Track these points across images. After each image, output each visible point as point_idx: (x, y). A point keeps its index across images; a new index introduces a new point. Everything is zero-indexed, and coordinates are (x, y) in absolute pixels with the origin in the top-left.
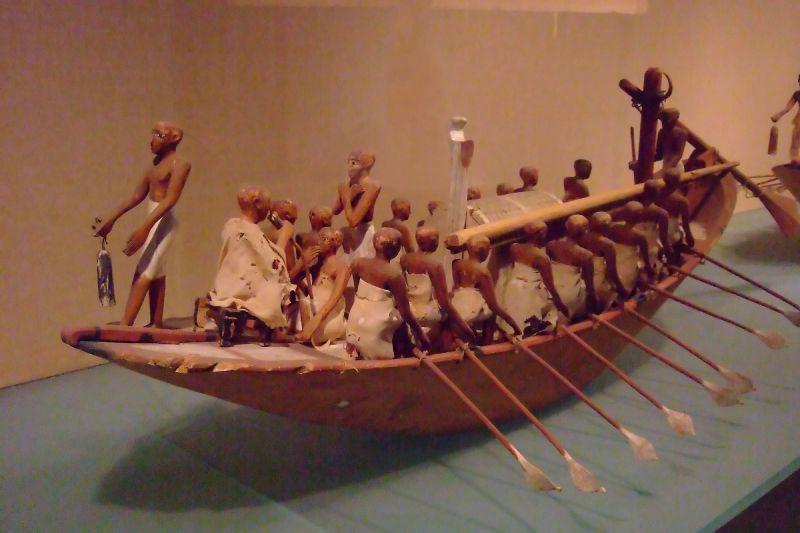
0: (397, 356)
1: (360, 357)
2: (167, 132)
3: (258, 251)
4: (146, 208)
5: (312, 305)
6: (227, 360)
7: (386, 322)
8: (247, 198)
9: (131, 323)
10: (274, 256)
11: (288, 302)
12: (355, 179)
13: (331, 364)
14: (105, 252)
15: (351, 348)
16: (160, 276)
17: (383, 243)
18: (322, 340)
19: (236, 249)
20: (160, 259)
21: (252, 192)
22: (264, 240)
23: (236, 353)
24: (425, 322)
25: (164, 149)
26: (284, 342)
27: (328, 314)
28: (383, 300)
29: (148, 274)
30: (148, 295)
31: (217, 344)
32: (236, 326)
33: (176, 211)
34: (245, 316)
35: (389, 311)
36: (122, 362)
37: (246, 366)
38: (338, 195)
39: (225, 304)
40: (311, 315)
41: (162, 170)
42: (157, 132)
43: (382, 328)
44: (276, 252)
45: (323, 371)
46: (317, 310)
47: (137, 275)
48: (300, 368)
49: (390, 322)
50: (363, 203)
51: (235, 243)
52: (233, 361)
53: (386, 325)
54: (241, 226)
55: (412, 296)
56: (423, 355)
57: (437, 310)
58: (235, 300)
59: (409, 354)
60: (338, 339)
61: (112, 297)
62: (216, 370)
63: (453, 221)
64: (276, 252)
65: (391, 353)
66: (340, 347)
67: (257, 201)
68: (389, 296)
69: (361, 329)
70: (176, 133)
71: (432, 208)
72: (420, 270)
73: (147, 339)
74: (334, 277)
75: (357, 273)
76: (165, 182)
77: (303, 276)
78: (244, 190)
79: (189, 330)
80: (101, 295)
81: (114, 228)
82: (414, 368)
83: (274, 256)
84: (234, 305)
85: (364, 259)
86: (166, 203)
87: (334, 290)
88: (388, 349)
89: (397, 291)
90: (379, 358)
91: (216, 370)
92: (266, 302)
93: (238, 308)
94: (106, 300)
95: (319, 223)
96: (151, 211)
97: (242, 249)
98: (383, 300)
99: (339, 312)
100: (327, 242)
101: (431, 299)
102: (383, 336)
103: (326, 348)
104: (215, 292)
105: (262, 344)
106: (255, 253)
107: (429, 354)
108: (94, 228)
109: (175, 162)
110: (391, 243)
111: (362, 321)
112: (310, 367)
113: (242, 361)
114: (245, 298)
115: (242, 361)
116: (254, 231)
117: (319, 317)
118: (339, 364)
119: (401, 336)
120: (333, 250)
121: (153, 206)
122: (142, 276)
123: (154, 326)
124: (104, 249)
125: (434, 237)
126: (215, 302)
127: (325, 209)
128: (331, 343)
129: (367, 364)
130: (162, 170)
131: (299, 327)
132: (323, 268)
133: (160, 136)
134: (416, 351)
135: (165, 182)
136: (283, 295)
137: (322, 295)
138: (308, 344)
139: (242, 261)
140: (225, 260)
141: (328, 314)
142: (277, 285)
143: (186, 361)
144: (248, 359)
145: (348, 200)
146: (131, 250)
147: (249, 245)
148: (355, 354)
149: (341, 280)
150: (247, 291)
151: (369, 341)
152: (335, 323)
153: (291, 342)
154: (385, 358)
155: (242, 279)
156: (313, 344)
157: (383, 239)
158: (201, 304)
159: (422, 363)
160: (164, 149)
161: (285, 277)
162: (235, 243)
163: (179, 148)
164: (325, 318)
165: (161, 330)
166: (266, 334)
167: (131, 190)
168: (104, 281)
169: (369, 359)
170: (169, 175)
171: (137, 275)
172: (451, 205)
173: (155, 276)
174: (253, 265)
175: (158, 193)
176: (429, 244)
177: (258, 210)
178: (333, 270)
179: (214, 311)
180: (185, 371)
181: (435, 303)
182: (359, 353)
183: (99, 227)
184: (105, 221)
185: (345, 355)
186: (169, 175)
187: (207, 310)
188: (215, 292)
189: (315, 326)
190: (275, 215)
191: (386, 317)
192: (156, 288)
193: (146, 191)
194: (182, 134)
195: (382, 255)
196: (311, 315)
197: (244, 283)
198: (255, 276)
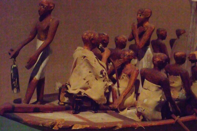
0: (163, 119)
1: (144, 120)
2: (47, 5)
3: (93, 65)
4: (35, 44)
5: (119, 91)
6: (78, 123)
7: (158, 102)
8: (87, 38)
9: (28, 103)
10: (101, 68)
11: (108, 91)
12: (141, 23)
13: (131, 124)
14: (15, 66)
15: (139, 114)
16: (42, 78)
17: (158, 62)
18: (123, 108)
19: (81, 64)
20: (43, 69)
21: (90, 34)
22: (96, 60)
23: (80, 118)
24: (178, 100)
25: (45, 13)
26: (104, 110)
27: (126, 95)
28: (157, 91)
29: (37, 77)
30: (36, 89)
31: (72, 111)
32: (80, 103)
33: (51, 46)
34: (87, 99)
35: (161, 96)
36: (26, 124)
37: (88, 126)
38: (131, 31)
39: (75, 92)
40: (118, 95)
41: (44, 24)
42: (42, 5)
43: (156, 104)
44: (101, 65)
45: (128, 127)
46: (121, 92)
47: (32, 78)
48: (115, 127)
49: (160, 102)
50: (145, 37)
51: (81, 61)
52: (82, 124)
53: (158, 104)
54: (82, 52)
55: (172, 87)
56: (177, 118)
57: (184, 95)
58: (81, 90)
59: (170, 118)
60: (132, 107)
61: (18, 89)
62: (73, 128)
63: (191, 43)
64: (101, 65)
65: (161, 117)
66: (133, 111)
67: (92, 39)
68: (160, 88)
69: (145, 105)
70: (51, 5)
71: (179, 33)
72: (176, 74)
73: (37, 110)
74: (129, 76)
75: (145, 75)
76: (46, 31)
77: (114, 74)
78: (85, 34)
79: (56, 103)
80: (13, 88)
81: (20, 54)
82: (171, 125)
83: (101, 68)
84: (80, 93)
85: (147, 69)
86: (48, 41)
87: (129, 83)
88: (158, 115)
89: (165, 86)
90: (154, 120)
91: (73, 128)
92: (96, 91)
93: (82, 94)
94: (15, 90)
95: (121, 45)
96: (38, 48)
97: (85, 63)
98: (157, 91)
99: (132, 93)
100: (126, 57)
101: (181, 89)
102: (156, 109)
103: (126, 112)
104: (69, 84)
105: (94, 112)
106: (91, 67)
107: (180, 117)
108: (10, 54)
109: (51, 20)
110: (162, 61)
111: (145, 101)
112: (120, 126)
113: (86, 124)
114: (85, 89)
115: (86, 124)
116: (91, 55)
117: (123, 97)
118: (134, 124)
119: (164, 108)
120: (129, 61)
121: (40, 43)
122: (34, 78)
123: (39, 103)
124: (15, 64)
125: (183, 57)
126: (71, 91)
127: (124, 36)
128: (128, 109)
129: (149, 124)
130: (44, 24)
131: (111, 100)
132: (123, 70)
133: (44, 7)
134: (173, 116)
135: (46, 31)
136: (105, 87)
137: (123, 84)
138: (116, 110)
139: (84, 70)
140: (75, 69)
141: (126, 95)
142: (102, 82)
143: (57, 123)
144: (89, 122)
145: (137, 33)
146: (29, 67)
147: (88, 63)
148: (141, 117)
149: (133, 78)
150: (87, 86)
151: (148, 111)
152: (131, 99)
153: (108, 109)
154: (158, 120)
155: (84, 79)
156: (119, 110)
157: (158, 59)
158: (62, 91)
159: (177, 122)
160: (45, 13)
161: (106, 78)
162: (81, 61)
163: (53, 13)
164: (125, 97)
165: (43, 103)
166: (95, 106)
167: (26, 35)
168: (15, 80)
169: (149, 120)
170: (48, 27)
171: (32, 78)
172: (190, 34)
173: (40, 77)
174: (90, 72)
175: (42, 36)
176: (180, 60)
177: (93, 44)
178: (128, 72)
179: (69, 95)
180: (57, 129)
181: (183, 91)
182: (143, 116)
183: (13, 53)
184: (16, 50)
185: (136, 118)
186: (48, 27)
187: (65, 93)
188: (69, 84)
189: (120, 101)
190: (101, 45)
191: (158, 99)
192: (41, 83)
193: (36, 33)
194: (54, 5)
195: (157, 68)
196: (118, 95)
197: (85, 81)
198: (91, 78)
